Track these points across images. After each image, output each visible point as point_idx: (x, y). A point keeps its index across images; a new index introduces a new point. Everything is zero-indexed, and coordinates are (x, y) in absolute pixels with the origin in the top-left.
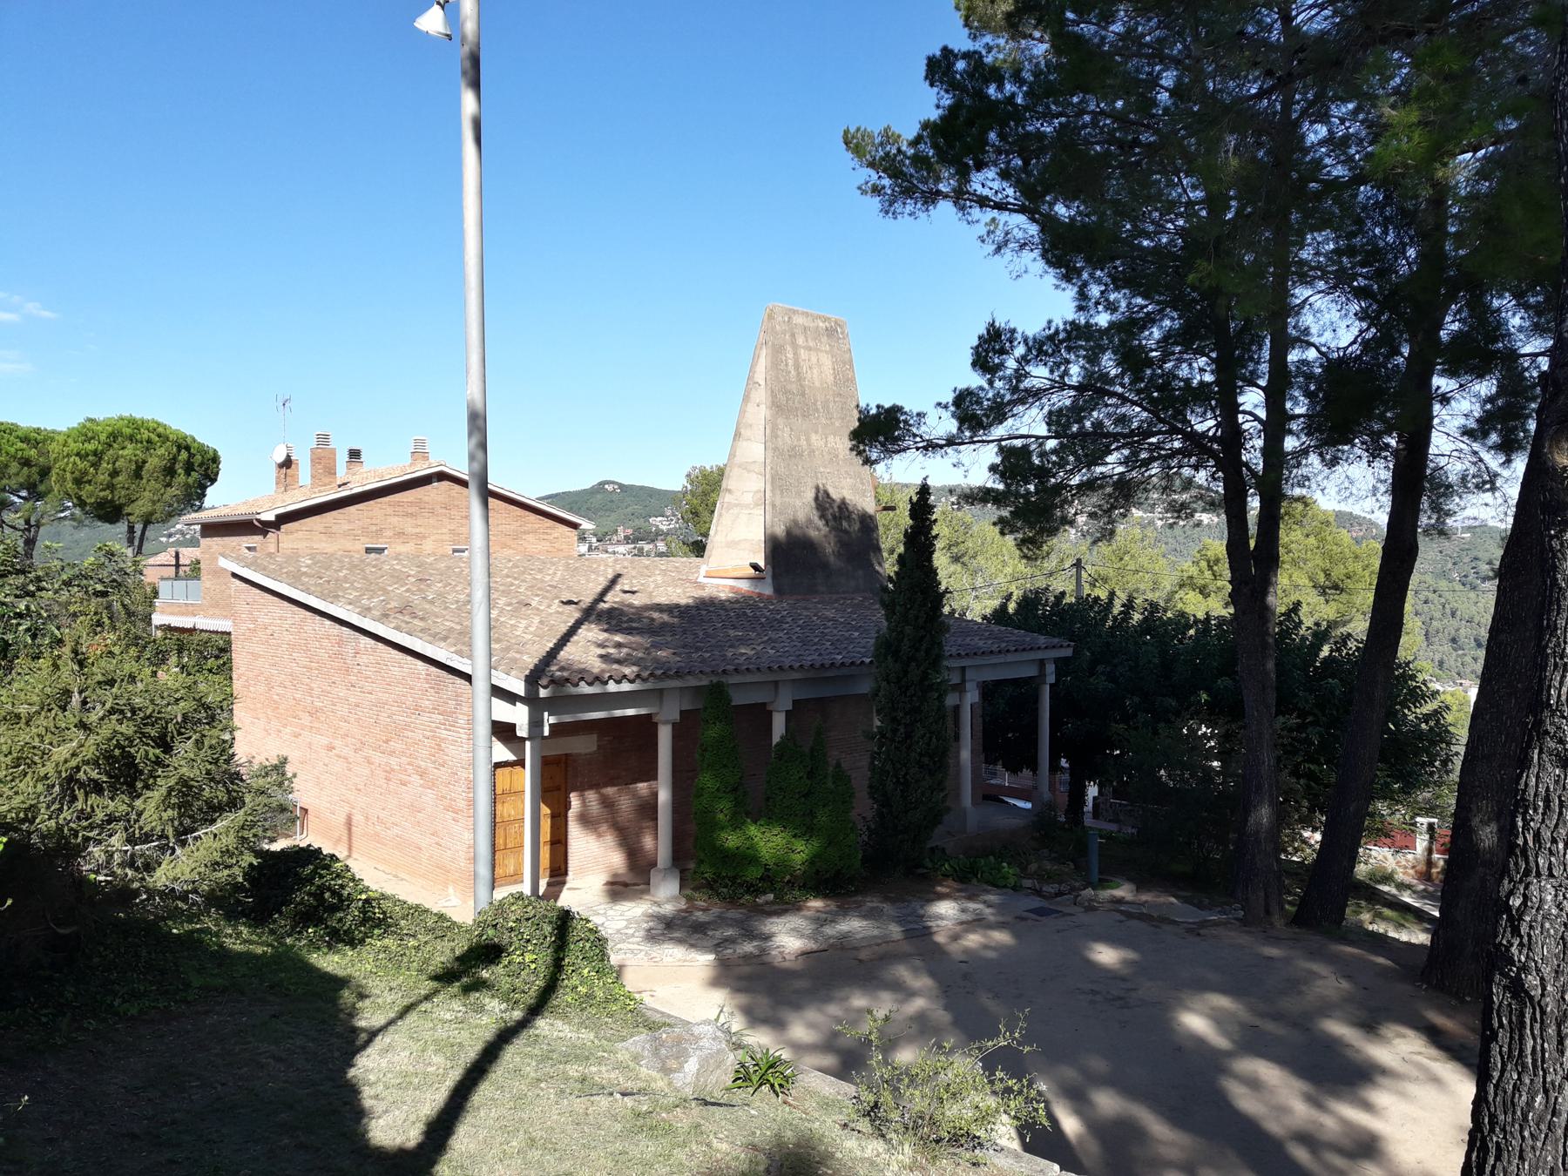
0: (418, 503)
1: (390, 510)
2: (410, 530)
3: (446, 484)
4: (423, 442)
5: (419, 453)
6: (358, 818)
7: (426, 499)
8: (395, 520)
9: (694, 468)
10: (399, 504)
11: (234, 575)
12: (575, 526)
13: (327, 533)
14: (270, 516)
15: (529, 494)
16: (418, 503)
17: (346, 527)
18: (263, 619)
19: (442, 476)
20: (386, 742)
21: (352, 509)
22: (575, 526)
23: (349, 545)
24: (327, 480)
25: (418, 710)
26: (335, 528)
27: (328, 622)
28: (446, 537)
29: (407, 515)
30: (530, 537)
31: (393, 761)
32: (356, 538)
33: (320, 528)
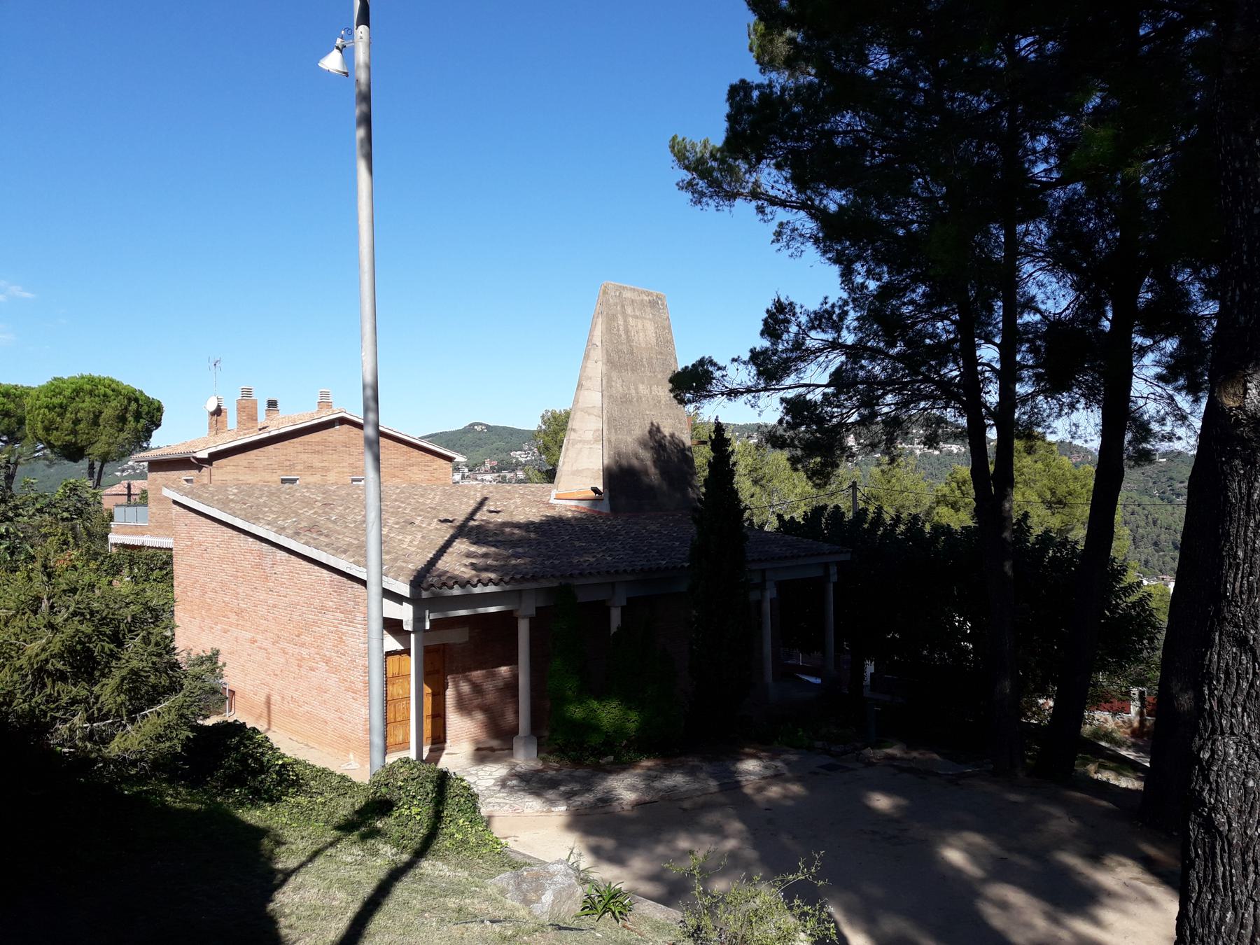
0: (324, 442)
1: (300, 449)
2: (317, 464)
3: (346, 427)
5: (324, 403)
6: (275, 698)
7: (330, 439)
8: (304, 457)
10: (308, 443)
11: (175, 502)
13: (251, 467)
15: (413, 435)
17: (266, 463)
18: (198, 537)
21: (270, 448)
22: (450, 459)
25: (323, 609)
26: (257, 464)
30: (415, 469)
31: (304, 651)
32: (273, 471)
33: (245, 463)
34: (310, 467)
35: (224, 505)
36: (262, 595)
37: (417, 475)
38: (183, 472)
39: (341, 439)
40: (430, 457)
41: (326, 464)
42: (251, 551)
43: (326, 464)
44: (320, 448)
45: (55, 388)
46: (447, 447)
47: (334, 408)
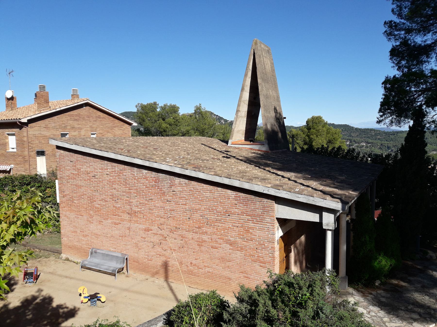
0: (79, 115)
1: (69, 118)
2: (76, 126)
3: (88, 108)
4: (76, 90)
5: (75, 95)
6: (171, 263)
7: (81, 113)
8: (71, 122)
9: (139, 104)
10: (72, 115)
11: (58, 147)
12: (130, 124)
13: (46, 127)
14: (25, 120)
15: (117, 111)
16: (79, 115)
17: (53, 125)
18: (84, 169)
19: (87, 104)
20: (199, 228)
21: (55, 117)
22: (130, 124)
23: (55, 133)
24: (45, 105)
25: (228, 213)
26: (49, 126)
27: (145, 171)
28: (89, 129)
29: (75, 120)
30: (116, 129)
31: (205, 237)
32: (57, 129)
33: (43, 125)
34: (73, 128)
35: (129, 153)
36: (159, 204)
37: (118, 132)
38: (7, 130)
39: (86, 113)
40: (122, 123)
41: (80, 126)
42: (146, 178)
43: (80, 126)
44: (76, 118)
45: (171, 105)
46: (128, 118)
47: (80, 98)
